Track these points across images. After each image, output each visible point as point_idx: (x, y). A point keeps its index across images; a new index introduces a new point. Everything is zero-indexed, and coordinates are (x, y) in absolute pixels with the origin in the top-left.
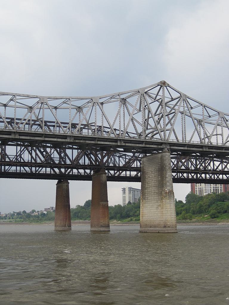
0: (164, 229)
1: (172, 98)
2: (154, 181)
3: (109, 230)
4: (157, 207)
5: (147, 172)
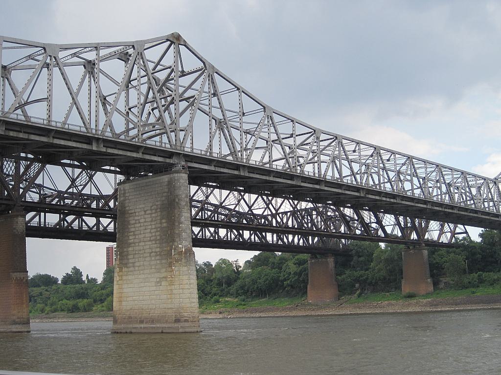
0: (176, 325)
1: (183, 71)
2: (152, 229)
3: (29, 330)
4: (158, 282)
5: (133, 211)
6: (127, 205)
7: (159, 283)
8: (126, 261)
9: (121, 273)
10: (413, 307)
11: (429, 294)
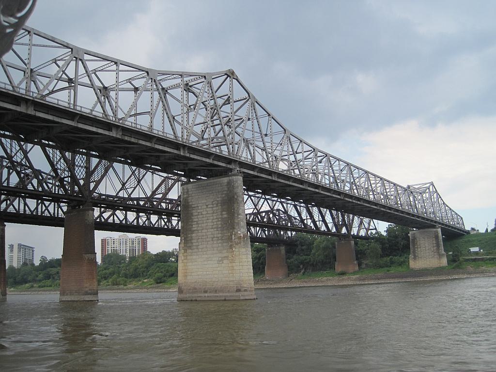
5: (196, 206)
6: (190, 201)
7: (221, 261)
8: (190, 245)
9: (185, 254)
10: (345, 281)
11: (356, 272)
